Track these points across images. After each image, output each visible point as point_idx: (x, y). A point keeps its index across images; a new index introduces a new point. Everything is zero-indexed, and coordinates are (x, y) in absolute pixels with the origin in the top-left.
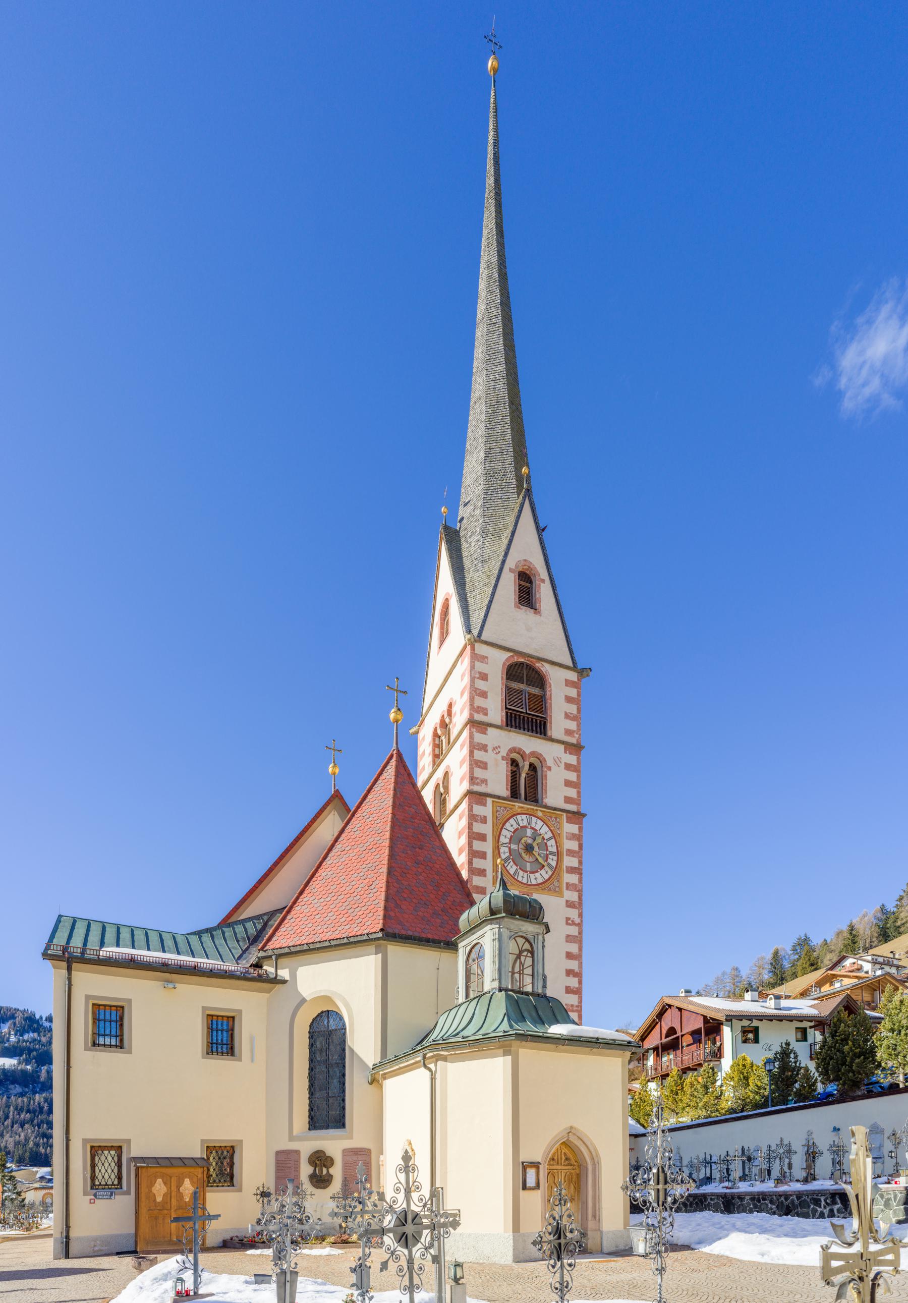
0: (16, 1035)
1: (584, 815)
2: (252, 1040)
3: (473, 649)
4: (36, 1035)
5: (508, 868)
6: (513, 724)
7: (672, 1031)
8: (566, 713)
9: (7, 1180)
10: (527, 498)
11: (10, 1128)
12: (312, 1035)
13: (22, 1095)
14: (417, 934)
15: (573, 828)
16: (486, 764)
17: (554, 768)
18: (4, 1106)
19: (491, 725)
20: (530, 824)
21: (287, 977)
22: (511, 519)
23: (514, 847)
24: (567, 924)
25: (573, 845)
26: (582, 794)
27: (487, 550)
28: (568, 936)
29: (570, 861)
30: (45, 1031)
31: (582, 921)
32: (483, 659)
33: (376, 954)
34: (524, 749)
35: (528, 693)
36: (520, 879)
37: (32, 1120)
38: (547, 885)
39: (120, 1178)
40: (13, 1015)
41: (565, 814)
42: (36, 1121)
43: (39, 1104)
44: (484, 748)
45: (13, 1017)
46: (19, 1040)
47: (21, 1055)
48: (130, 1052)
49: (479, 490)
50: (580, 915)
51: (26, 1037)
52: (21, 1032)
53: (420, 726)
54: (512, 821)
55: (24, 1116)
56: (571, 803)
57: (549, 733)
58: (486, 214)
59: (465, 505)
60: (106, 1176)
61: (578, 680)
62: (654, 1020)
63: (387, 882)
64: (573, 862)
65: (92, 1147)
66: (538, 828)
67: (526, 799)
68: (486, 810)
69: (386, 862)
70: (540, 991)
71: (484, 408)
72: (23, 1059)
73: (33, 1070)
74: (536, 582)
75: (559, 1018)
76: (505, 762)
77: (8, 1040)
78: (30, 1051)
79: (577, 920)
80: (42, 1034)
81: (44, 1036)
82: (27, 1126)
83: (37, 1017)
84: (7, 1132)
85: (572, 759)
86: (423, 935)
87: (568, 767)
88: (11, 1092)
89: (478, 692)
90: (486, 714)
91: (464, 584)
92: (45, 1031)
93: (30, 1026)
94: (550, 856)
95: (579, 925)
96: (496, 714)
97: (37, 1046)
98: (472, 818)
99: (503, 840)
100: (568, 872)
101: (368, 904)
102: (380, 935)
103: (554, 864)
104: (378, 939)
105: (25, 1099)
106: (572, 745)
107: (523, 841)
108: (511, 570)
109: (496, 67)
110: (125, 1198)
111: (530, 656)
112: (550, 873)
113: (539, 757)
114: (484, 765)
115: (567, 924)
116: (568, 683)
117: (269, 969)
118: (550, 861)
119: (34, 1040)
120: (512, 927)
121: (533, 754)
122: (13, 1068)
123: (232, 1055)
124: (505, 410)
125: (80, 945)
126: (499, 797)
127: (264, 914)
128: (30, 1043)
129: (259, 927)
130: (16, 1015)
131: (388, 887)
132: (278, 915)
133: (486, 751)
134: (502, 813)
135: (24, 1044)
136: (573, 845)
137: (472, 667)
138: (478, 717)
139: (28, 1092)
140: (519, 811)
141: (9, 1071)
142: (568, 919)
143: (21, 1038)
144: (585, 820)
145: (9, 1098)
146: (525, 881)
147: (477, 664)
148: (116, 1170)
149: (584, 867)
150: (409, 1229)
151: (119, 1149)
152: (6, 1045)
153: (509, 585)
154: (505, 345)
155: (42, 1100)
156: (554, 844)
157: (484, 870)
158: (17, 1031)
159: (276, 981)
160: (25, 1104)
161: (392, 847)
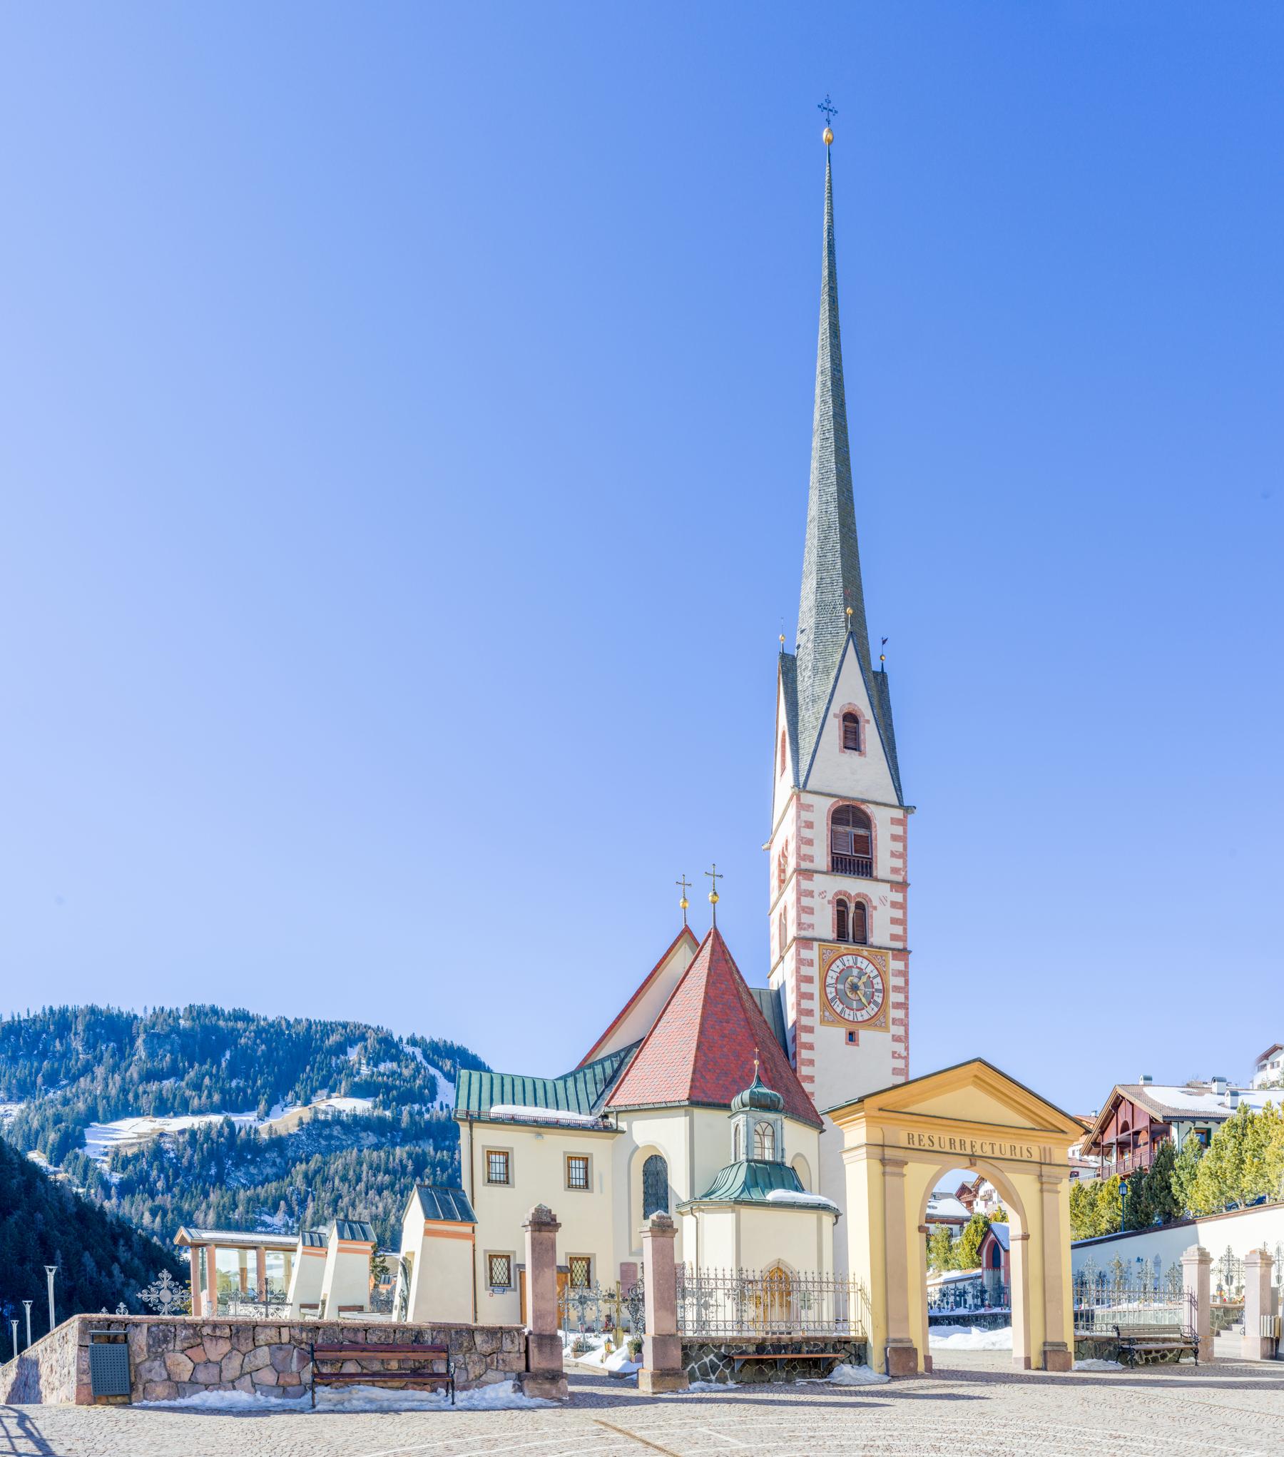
0: (368, 1064)
1: (910, 952)
2: (601, 1176)
3: (798, 798)
4: (395, 1065)
5: (835, 1007)
6: (840, 867)
7: (1125, 1127)
8: (892, 852)
9: (379, 1272)
10: (851, 640)
11: (363, 1195)
12: (645, 1173)
13: (377, 1147)
14: (716, 1101)
15: (899, 965)
16: (812, 909)
17: (880, 907)
18: (354, 1163)
19: (817, 872)
20: (856, 964)
21: (625, 1129)
22: (838, 657)
23: (840, 986)
24: (894, 1057)
25: (900, 981)
26: (908, 931)
27: (816, 689)
28: (894, 1069)
29: (895, 997)
30: (407, 1060)
31: (908, 1054)
32: (809, 807)
33: (686, 1116)
34: (849, 891)
35: (855, 835)
36: (846, 1017)
37: (392, 1185)
38: (873, 1021)
39: (509, 1278)
40: (363, 1034)
41: (890, 952)
42: (397, 1186)
43: (401, 1161)
44: (810, 894)
45: (363, 1038)
46: (373, 1073)
47: (376, 1096)
48: (514, 1187)
49: (812, 622)
50: (907, 1049)
51: (382, 1067)
52: (375, 1060)
53: (771, 843)
54: (838, 962)
55: (383, 1178)
56: (897, 940)
57: (874, 874)
58: (822, 311)
59: (802, 632)
60: (500, 1278)
61: (904, 817)
62: (1110, 1111)
63: (696, 1056)
64: (899, 998)
65: (490, 1256)
66: (863, 967)
67: (854, 942)
68: (813, 954)
69: (696, 1038)
70: (779, 1160)
71: (817, 533)
72: (380, 1101)
73: (393, 1118)
74: (861, 720)
75: (786, 1183)
76: (831, 906)
77: (358, 1073)
78: (388, 1089)
79: (904, 1054)
80: (403, 1064)
81: (406, 1067)
82: (386, 1193)
83: (396, 1039)
84: (361, 1201)
85: (898, 897)
86: (722, 1101)
87: (894, 905)
88: (363, 1142)
89: (804, 840)
90: (812, 861)
91: (797, 723)
92: (407, 1060)
93: (386, 1052)
94: (876, 994)
95: (906, 1058)
96: (822, 859)
97: (398, 1082)
98: (800, 962)
99: (829, 981)
100: (894, 1008)
101: (681, 1074)
102: (687, 1103)
103: (880, 1000)
104: (685, 1106)
105: (382, 1154)
106: (898, 883)
107: (849, 980)
108: (835, 716)
109: (831, 138)
110: (513, 1293)
111: (854, 799)
112: (876, 1009)
113: (864, 896)
114: (810, 911)
115: (894, 1057)
116: (895, 821)
117: (612, 1120)
118: (875, 998)
119: (393, 1073)
120: (756, 1116)
121: (858, 895)
122: (367, 1114)
123: (587, 1188)
124: (835, 537)
125: (477, 1109)
126: (824, 941)
127: (622, 1050)
128: (388, 1078)
129: (616, 1065)
130: (368, 1035)
131: (696, 1061)
132: (635, 1049)
133: (813, 897)
134: (829, 956)
135: (380, 1078)
136: (900, 981)
137: (798, 817)
138: (805, 865)
139: (385, 1143)
140: (845, 952)
141: (361, 1118)
142: (894, 1053)
143: (375, 1069)
144: (910, 956)
145: (360, 1151)
146: (851, 1019)
147: (803, 813)
148: (506, 1273)
149: (910, 1002)
150: (583, 1300)
151: (508, 1257)
152: (356, 1079)
153: (834, 729)
154: (836, 463)
155: (405, 1156)
156: (880, 981)
157: (812, 1010)
158: (369, 1059)
159: (617, 1131)
160: (383, 1162)
161: (702, 1025)
